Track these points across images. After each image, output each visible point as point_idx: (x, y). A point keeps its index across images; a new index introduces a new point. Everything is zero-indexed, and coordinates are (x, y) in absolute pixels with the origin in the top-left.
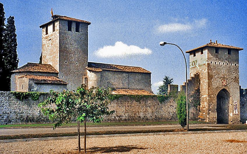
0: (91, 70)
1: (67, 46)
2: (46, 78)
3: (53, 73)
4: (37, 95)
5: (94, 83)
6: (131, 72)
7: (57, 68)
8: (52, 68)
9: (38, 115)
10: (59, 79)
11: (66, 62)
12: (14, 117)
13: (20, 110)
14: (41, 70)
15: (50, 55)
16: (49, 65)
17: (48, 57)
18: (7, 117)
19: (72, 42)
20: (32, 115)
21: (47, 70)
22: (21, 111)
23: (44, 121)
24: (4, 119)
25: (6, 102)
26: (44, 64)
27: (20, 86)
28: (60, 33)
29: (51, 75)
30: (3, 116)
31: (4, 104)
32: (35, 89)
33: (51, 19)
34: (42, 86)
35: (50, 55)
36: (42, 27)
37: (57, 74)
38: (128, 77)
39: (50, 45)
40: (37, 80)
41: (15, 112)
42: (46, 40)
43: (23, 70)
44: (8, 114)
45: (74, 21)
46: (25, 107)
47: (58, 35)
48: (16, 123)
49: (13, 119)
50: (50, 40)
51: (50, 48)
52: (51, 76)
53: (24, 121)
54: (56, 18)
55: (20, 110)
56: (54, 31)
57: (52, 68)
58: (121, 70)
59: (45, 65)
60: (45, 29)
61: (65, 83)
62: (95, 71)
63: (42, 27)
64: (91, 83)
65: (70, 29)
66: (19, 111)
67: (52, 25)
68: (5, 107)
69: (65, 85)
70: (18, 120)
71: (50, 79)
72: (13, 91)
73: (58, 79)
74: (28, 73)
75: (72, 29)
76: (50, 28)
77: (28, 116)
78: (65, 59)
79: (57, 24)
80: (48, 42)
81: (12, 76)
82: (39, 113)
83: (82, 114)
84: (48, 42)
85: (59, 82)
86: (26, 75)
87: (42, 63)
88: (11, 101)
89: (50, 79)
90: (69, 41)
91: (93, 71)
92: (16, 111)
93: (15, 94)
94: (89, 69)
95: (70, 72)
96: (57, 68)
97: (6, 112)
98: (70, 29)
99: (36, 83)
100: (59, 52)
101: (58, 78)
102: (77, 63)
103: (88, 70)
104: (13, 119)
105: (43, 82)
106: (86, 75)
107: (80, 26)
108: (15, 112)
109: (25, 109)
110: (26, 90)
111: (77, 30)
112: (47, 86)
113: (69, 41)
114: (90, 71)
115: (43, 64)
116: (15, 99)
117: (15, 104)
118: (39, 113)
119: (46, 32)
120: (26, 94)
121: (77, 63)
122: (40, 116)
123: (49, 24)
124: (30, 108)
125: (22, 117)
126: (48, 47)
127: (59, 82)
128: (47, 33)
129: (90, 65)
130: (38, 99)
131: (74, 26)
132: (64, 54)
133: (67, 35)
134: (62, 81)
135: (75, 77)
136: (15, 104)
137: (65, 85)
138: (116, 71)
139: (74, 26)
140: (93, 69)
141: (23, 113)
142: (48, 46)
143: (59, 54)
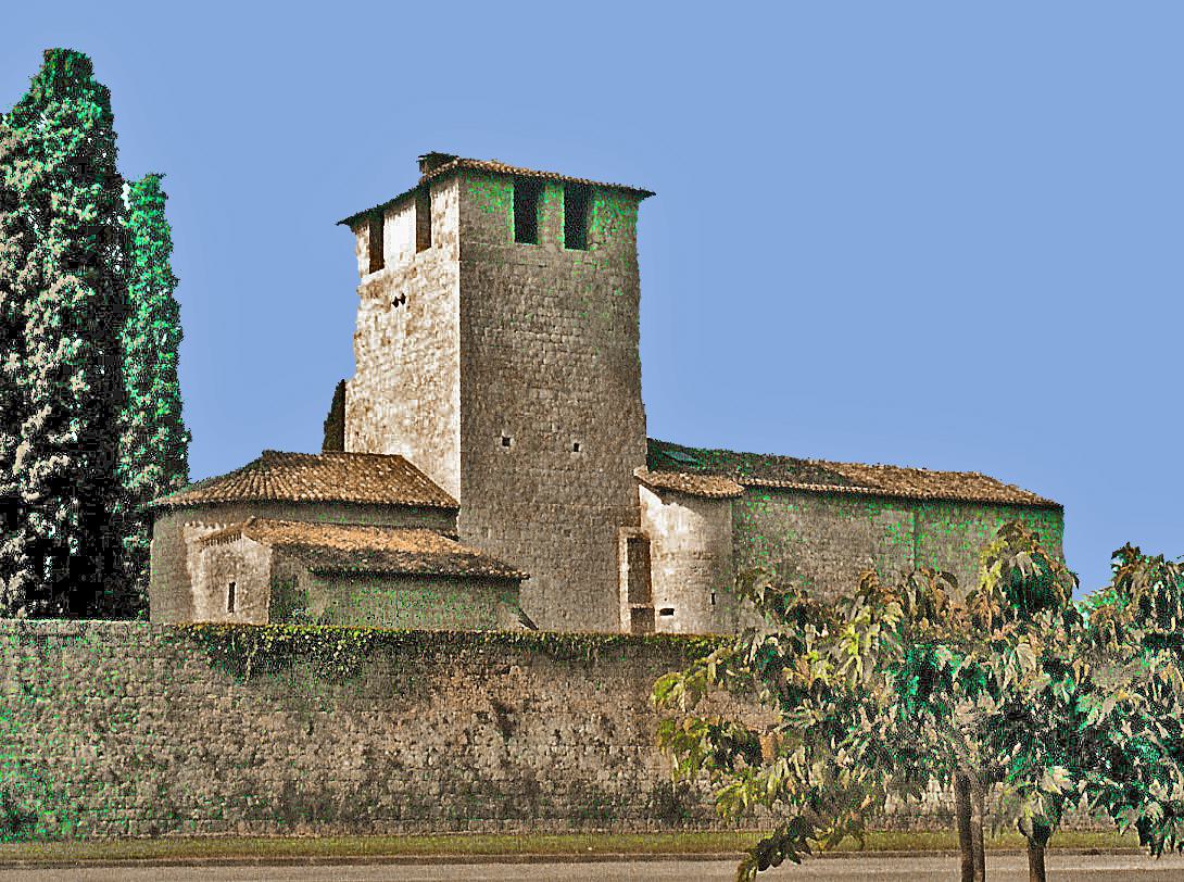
0: (672, 491)
1: (514, 337)
2: (379, 541)
3: (423, 509)
4: (350, 647)
5: (695, 569)
6: (931, 501)
7: (449, 474)
8: (413, 478)
9: (356, 774)
10: (464, 543)
11: (506, 442)
12: (205, 789)
13: (240, 744)
14: (348, 490)
15: (401, 393)
16: (394, 457)
17: (384, 410)
18: (160, 789)
19: (541, 311)
20: (315, 774)
21: (386, 488)
22: (247, 749)
23: (398, 818)
24: (140, 800)
25: (151, 692)
26: (362, 455)
27: (214, 588)
28: (467, 258)
29: (411, 520)
30: (132, 782)
31: (136, 707)
32: (317, 609)
33: (413, 178)
34: (360, 592)
35: (401, 393)
36: (354, 222)
37: (450, 512)
38: (915, 535)
39: (401, 335)
40: (323, 553)
41: (207, 754)
42: (376, 301)
43: (232, 491)
44: (165, 765)
45: (556, 182)
46: (274, 723)
47: (454, 268)
48: (213, 830)
49: (196, 805)
50: (396, 304)
51: (399, 353)
52: (413, 528)
53: (267, 817)
54: (440, 169)
55: (240, 744)
56: (424, 241)
57: (413, 478)
58: (865, 484)
59: (372, 459)
60: (363, 241)
61: (511, 569)
62: (696, 497)
63: (354, 222)
64: (669, 571)
65: (527, 230)
66: (232, 748)
67: (414, 210)
68: (142, 726)
69: (506, 583)
70: (229, 806)
71: (407, 544)
72: (164, 614)
73: (458, 549)
74: (262, 512)
75: (544, 230)
76: (400, 230)
77: (290, 786)
78: (499, 422)
79: (447, 205)
80: (383, 318)
81: (161, 526)
82: (361, 761)
83: (1037, 772)
84: (383, 318)
85: (470, 566)
86: (254, 520)
87: (343, 449)
88: (181, 683)
89: (407, 544)
90: (522, 308)
91: (683, 497)
92: (211, 747)
93: (207, 636)
94: (657, 478)
95: (528, 500)
96: (449, 474)
97: (149, 757)
98: (527, 230)
99: (319, 574)
100: (458, 377)
101: (455, 538)
102: (576, 446)
103: (648, 486)
104: (196, 805)
105: (365, 565)
106: (633, 516)
107: (595, 212)
108: (207, 754)
109: (273, 736)
110: (249, 615)
111: (576, 235)
112: (391, 594)
113: (522, 308)
114: (663, 492)
115: (355, 455)
116: (208, 672)
117: (211, 706)
118: (361, 761)
119: (372, 256)
120: (281, 638)
121: (576, 446)
122: (368, 783)
123: (396, 206)
124: (304, 736)
125: (251, 787)
126: (386, 349)
127: (470, 566)
128: (377, 262)
129: (660, 456)
130: (356, 672)
131: (552, 211)
132: (494, 388)
133: (512, 265)
134: (484, 559)
135: (567, 533)
136: (211, 706)
137: (506, 583)
138: (834, 494)
139: (552, 211)
140: (683, 480)
141: (263, 761)
142: (386, 342)
143: (457, 387)
